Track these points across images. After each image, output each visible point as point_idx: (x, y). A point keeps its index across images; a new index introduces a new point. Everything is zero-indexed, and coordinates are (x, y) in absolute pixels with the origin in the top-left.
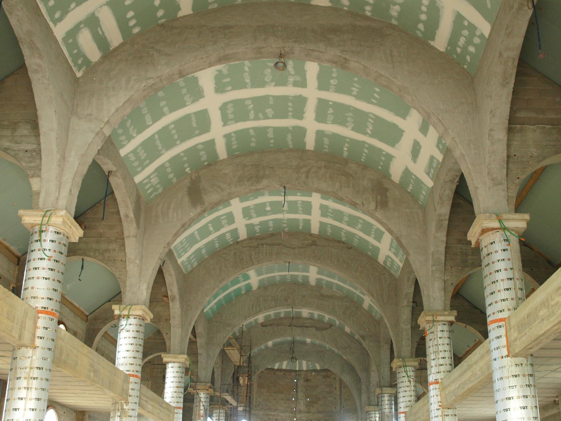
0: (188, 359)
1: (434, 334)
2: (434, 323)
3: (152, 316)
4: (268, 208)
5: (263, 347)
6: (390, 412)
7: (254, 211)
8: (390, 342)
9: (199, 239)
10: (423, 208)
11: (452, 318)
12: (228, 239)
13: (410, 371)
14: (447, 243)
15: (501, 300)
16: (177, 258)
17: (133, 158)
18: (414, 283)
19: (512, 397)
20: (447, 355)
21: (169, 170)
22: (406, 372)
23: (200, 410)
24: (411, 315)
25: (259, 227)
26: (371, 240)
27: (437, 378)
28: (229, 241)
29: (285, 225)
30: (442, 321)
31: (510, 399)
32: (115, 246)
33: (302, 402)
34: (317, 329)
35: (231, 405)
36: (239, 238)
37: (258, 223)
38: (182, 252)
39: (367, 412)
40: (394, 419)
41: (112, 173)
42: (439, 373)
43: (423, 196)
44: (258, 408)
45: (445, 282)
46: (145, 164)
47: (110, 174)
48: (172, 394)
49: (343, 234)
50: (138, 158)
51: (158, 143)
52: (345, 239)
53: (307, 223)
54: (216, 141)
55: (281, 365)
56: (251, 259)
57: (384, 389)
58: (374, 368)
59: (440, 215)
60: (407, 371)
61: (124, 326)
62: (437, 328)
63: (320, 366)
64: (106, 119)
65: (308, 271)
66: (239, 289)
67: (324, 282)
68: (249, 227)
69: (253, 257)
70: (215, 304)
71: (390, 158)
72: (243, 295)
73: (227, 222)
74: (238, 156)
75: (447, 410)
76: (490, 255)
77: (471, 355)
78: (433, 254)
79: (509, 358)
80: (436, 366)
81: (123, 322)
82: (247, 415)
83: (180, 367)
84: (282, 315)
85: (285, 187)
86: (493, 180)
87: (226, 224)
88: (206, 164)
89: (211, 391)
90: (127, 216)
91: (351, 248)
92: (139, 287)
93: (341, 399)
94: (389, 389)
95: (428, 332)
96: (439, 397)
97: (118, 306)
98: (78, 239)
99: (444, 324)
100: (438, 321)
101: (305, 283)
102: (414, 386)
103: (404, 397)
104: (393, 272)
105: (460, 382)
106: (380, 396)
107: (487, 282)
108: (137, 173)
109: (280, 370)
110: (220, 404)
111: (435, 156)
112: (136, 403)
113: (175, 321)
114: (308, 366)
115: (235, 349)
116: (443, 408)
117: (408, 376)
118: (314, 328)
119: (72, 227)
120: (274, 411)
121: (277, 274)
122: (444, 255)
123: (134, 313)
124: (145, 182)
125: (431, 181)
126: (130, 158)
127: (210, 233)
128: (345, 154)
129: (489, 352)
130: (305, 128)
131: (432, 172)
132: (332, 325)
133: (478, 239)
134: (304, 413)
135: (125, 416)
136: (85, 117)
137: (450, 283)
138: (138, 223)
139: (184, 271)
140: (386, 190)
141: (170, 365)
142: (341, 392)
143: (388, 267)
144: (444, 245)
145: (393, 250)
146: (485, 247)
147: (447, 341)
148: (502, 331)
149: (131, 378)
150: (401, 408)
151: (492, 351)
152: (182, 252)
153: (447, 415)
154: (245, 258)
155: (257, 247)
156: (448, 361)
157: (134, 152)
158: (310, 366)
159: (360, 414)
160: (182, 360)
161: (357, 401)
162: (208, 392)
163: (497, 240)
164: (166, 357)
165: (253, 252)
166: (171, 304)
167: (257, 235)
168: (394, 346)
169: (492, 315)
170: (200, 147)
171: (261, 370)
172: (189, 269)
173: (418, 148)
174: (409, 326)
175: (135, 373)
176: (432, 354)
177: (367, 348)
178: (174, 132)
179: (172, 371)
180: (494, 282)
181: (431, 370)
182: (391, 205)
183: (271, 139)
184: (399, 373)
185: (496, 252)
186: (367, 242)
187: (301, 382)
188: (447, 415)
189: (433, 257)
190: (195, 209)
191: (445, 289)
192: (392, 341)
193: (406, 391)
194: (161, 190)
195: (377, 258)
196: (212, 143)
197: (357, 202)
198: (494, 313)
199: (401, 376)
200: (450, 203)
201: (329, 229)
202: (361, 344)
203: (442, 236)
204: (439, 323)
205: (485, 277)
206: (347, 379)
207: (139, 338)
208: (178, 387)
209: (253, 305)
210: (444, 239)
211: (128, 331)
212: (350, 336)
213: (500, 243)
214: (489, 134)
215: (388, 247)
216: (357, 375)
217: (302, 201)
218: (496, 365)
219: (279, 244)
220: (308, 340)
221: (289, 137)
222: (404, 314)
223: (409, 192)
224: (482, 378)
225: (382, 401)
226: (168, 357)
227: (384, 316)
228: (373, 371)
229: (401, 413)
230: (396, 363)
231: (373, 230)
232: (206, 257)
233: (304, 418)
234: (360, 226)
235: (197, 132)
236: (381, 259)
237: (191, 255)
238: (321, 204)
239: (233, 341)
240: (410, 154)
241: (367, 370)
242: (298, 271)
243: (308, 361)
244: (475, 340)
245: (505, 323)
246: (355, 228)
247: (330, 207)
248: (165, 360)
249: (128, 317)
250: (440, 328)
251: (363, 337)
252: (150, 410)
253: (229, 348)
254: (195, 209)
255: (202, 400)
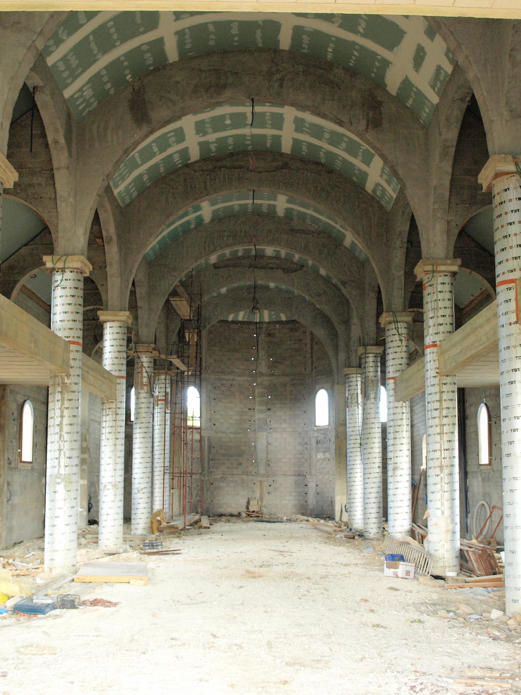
0: (131, 317)
1: (434, 288)
2: (434, 274)
3: (91, 267)
4: (228, 122)
5: (215, 294)
6: (375, 376)
7: (210, 126)
8: (377, 289)
9: (139, 161)
10: (426, 128)
11: (455, 268)
12: (176, 162)
13: (401, 328)
14: (453, 175)
15: (513, 258)
16: (113, 188)
17: (62, 67)
18: (410, 218)
19: (519, 369)
20: (448, 312)
21: (106, 79)
22: (397, 328)
23: (142, 377)
24: (404, 258)
25: (216, 145)
26: (357, 162)
27: (435, 340)
28: (177, 163)
29: (249, 142)
30: (444, 271)
31: (516, 370)
32: (40, 179)
33: (263, 363)
34: (286, 271)
35: (178, 368)
36: (189, 159)
37: (214, 140)
38: (119, 181)
39: (345, 376)
40: (379, 384)
41: (39, 89)
42: (437, 334)
43: (425, 113)
44: (209, 371)
45: (448, 223)
46: (76, 73)
47: (35, 90)
48: (113, 361)
49: (322, 154)
50: (68, 67)
51: (93, 46)
52: (325, 161)
53: (277, 140)
54: (166, 40)
55: (237, 316)
56: (205, 187)
57: (368, 347)
58: (355, 320)
59: (445, 141)
60: (398, 328)
61: (59, 282)
62: (437, 280)
63: (286, 316)
64: (39, 30)
65: (275, 199)
66: (188, 223)
67: (295, 213)
68: (204, 146)
69: (208, 183)
70: (158, 242)
71: (386, 63)
72: (192, 230)
73: (175, 140)
74: (191, 58)
75: (445, 378)
76: (503, 204)
77: (475, 317)
78: (435, 189)
79: (518, 325)
80: (434, 326)
81: (58, 277)
82: (198, 382)
83: (121, 327)
84: (240, 254)
85: (252, 100)
86: (511, 111)
87: (174, 142)
88: (151, 68)
89: (156, 353)
90: (56, 142)
91: (331, 172)
92: (75, 232)
93: (312, 357)
94: (374, 348)
95: (426, 285)
96: (437, 363)
97: (50, 257)
98: (12, 184)
99: (446, 276)
100: (439, 272)
101: (272, 212)
102: (406, 346)
103: (394, 359)
104: (383, 203)
105: (461, 347)
106: (364, 356)
107: (497, 223)
108: (67, 86)
109: (234, 322)
110: (166, 369)
111: (442, 66)
112: (79, 376)
113: (113, 270)
114: (270, 316)
115: (183, 299)
116: (441, 376)
117: (399, 334)
118: (281, 271)
119: (7, 170)
120: (229, 374)
121: (236, 203)
122: (449, 190)
123: (71, 265)
124: (76, 96)
125: (436, 96)
126: (59, 67)
127: (154, 155)
128: (330, 56)
129: (496, 315)
130: (279, 23)
131: (438, 86)
132: (303, 266)
133: (491, 184)
134: (267, 376)
135: (68, 392)
136: (12, 26)
137: (453, 224)
138: (70, 151)
139: (122, 205)
140: (380, 103)
141: (108, 325)
142: (312, 348)
143: (378, 196)
144: (449, 177)
145: (385, 177)
146: (498, 194)
147: (448, 296)
148: (512, 295)
149: (71, 345)
150: (389, 372)
151: (500, 317)
152: (119, 181)
153: (445, 384)
154: (197, 186)
155: (212, 171)
156: (448, 320)
157: (64, 59)
158: (274, 317)
159: (336, 377)
160: (124, 318)
161: (333, 360)
162: (152, 355)
163: (511, 186)
164: (103, 315)
165: (208, 177)
166: (106, 247)
167: (213, 154)
168: (383, 297)
169: (501, 275)
170: (145, 48)
171: (211, 324)
172: (128, 201)
173: (422, 54)
174: (402, 272)
175: (76, 340)
176: (431, 311)
177: (348, 296)
178: (113, 30)
179: (111, 332)
180: (506, 236)
181: (428, 331)
182: (385, 124)
183: (236, 35)
184: (388, 330)
185: (510, 200)
186: (353, 165)
187: (263, 337)
188: (445, 384)
189: (435, 192)
190: (140, 130)
191: (448, 232)
192: (379, 288)
193: (396, 352)
194: (95, 105)
195: (365, 185)
196: (160, 42)
197: (343, 119)
198: (504, 273)
199: (391, 334)
200: (459, 126)
201: (305, 147)
202: (339, 290)
203: (447, 166)
204: (440, 274)
205: (496, 230)
206: (320, 333)
207: (78, 297)
208: (119, 352)
209: (205, 243)
210: (450, 170)
211: (64, 288)
212: (327, 280)
213: (515, 190)
214: (510, 55)
215: (380, 174)
216: (333, 327)
217: (272, 113)
218: (503, 332)
219: (241, 167)
220: (272, 285)
221: (259, 33)
222: (397, 257)
223: (408, 107)
224: (487, 344)
225: (366, 363)
226: (106, 315)
227: (371, 259)
228: (354, 324)
229: (389, 378)
230: (384, 319)
231: (361, 151)
232: (149, 184)
233: (266, 383)
234: (344, 145)
235: (142, 29)
236: (369, 187)
237: (129, 184)
238: (296, 116)
239: (180, 290)
240: (412, 60)
241: (347, 322)
242: (262, 199)
243: (270, 311)
244: (481, 289)
245: (516, 285)
246: (338, 148)
247: (306, 121)
248: (102, 318)
249: (63, 270)
250: (440, 280)
251: (343, 283)
252: (92, 383)
253: (175, 299)
254: (140, 130)
255: (145, 364)
